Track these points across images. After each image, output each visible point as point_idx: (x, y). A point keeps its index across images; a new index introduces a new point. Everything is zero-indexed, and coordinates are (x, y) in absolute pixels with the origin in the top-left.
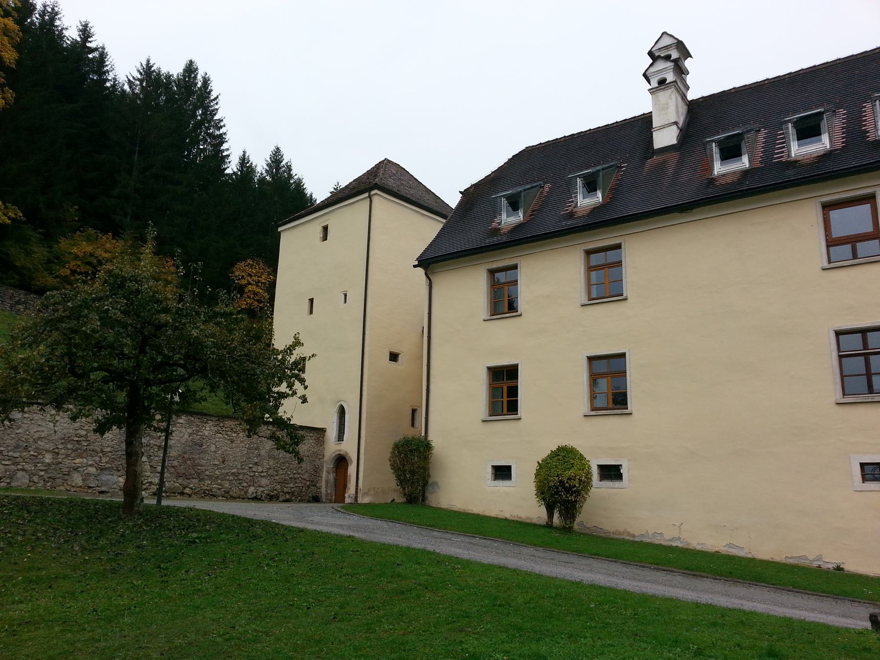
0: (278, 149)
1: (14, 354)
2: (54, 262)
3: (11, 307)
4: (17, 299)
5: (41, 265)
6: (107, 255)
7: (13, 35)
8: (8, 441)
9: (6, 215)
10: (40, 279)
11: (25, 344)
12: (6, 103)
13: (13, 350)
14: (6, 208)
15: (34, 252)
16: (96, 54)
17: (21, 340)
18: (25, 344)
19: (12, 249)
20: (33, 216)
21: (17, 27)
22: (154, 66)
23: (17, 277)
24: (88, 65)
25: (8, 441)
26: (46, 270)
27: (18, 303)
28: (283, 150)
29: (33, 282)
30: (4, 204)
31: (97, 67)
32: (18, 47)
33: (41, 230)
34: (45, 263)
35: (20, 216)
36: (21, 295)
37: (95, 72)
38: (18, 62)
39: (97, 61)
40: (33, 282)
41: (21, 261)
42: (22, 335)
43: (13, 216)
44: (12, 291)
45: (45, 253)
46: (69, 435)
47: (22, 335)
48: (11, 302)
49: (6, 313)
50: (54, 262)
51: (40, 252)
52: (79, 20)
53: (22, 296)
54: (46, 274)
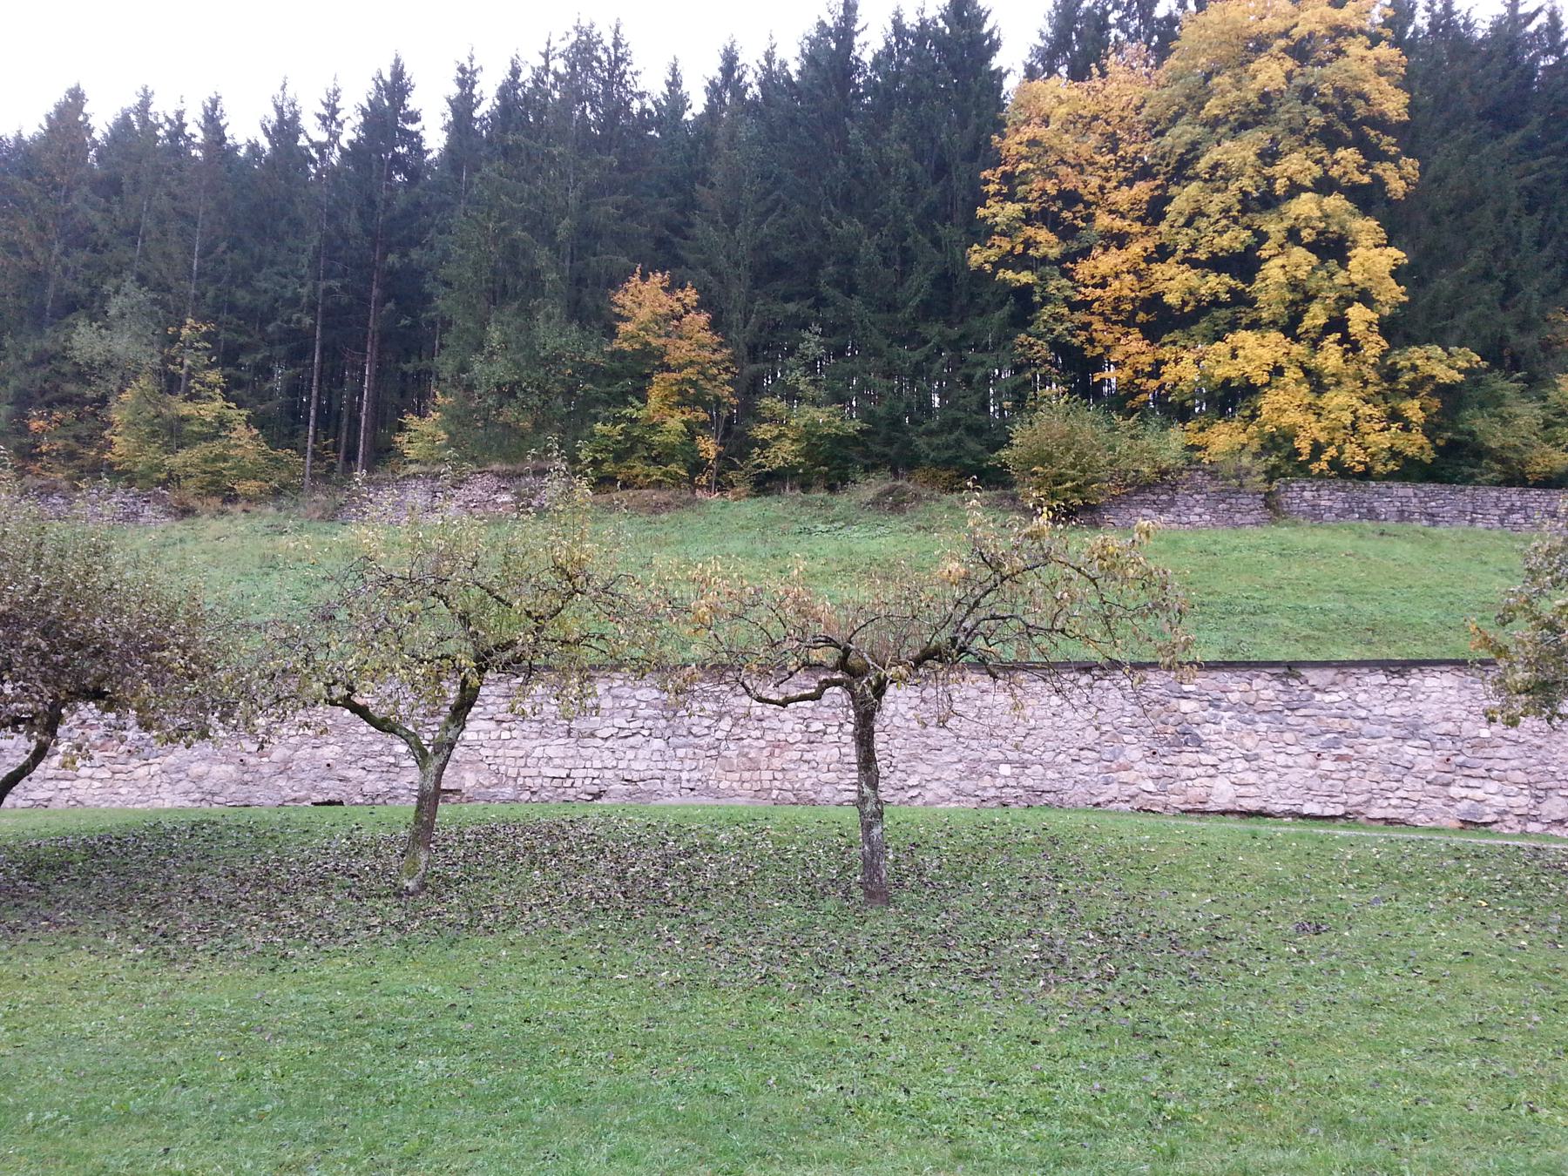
0: (398, 73)
1: (1544, 602)
2: (1557, 424)
3: (1501, 521)
4: (1508, 504)
5: (1535, 434)
6: (118, 459)
7: (1393, 68)
8: (1559, 755)
9: (1452, 368)
10: (1540, 460)
11: (1559, 580)
12: (1408, 184)
13: (1540, 592)
14: (1450, 355)
15: (1516, 416)
16: (1542, 19)
17: (1551, 574)
18: (1559, 580)
19: (1478, 422)
20: (1499, 355)
21: (1396, 51)
22: (822, 18)
23: (1497, 467)
24: (1530, 47)
25: (1559, 755)
26: (1547, 441)
27: (1511, 511)
28: (405, 60)
29: (1528, 469)
30: (1445, 349)
31: (1550, 40)
32: (1405, 84)
33: (1519, 375)
34: (1541, 430)
35: (1477, 362)
36: (1513, 496)
37: (1546, 53)
38: (1412, 108)
39: (1548, 29)
40: (1528, 469)
41: (1495, 438)
42: (1550, 564)
43: (1466, 365)
44: (1495, 494)
45: (1537, 411)
46: (258, 819)
47: (1550, 564)
48: (1498, 512)
49: (1496, 533)
50: (1557, 424)
51: (1528, 414)
52: (890, 9)
53: (1515, 497)
54: (1547, 448)
